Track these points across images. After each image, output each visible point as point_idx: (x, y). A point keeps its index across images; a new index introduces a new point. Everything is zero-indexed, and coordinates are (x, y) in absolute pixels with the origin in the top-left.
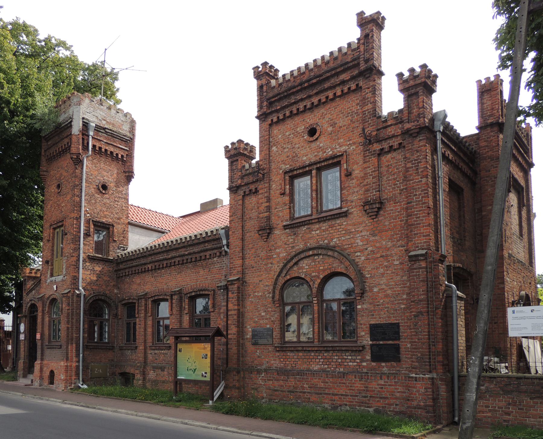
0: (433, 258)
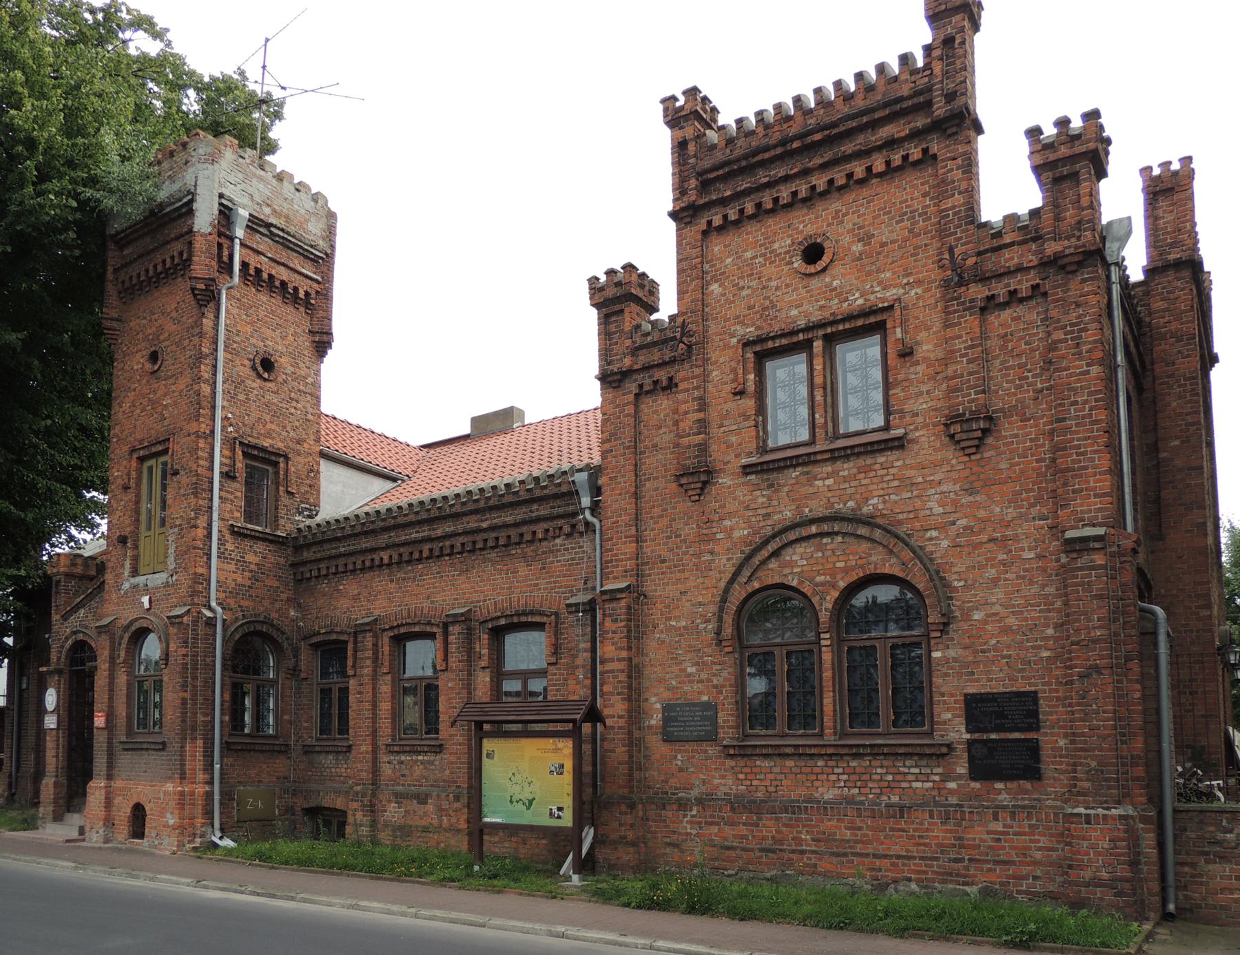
0: (1119, 546)
